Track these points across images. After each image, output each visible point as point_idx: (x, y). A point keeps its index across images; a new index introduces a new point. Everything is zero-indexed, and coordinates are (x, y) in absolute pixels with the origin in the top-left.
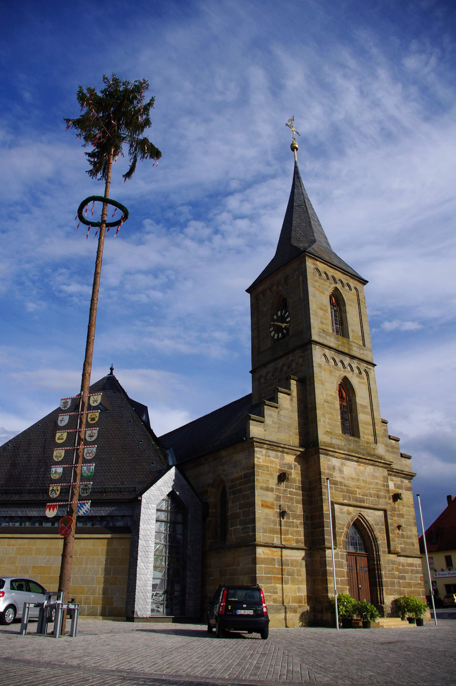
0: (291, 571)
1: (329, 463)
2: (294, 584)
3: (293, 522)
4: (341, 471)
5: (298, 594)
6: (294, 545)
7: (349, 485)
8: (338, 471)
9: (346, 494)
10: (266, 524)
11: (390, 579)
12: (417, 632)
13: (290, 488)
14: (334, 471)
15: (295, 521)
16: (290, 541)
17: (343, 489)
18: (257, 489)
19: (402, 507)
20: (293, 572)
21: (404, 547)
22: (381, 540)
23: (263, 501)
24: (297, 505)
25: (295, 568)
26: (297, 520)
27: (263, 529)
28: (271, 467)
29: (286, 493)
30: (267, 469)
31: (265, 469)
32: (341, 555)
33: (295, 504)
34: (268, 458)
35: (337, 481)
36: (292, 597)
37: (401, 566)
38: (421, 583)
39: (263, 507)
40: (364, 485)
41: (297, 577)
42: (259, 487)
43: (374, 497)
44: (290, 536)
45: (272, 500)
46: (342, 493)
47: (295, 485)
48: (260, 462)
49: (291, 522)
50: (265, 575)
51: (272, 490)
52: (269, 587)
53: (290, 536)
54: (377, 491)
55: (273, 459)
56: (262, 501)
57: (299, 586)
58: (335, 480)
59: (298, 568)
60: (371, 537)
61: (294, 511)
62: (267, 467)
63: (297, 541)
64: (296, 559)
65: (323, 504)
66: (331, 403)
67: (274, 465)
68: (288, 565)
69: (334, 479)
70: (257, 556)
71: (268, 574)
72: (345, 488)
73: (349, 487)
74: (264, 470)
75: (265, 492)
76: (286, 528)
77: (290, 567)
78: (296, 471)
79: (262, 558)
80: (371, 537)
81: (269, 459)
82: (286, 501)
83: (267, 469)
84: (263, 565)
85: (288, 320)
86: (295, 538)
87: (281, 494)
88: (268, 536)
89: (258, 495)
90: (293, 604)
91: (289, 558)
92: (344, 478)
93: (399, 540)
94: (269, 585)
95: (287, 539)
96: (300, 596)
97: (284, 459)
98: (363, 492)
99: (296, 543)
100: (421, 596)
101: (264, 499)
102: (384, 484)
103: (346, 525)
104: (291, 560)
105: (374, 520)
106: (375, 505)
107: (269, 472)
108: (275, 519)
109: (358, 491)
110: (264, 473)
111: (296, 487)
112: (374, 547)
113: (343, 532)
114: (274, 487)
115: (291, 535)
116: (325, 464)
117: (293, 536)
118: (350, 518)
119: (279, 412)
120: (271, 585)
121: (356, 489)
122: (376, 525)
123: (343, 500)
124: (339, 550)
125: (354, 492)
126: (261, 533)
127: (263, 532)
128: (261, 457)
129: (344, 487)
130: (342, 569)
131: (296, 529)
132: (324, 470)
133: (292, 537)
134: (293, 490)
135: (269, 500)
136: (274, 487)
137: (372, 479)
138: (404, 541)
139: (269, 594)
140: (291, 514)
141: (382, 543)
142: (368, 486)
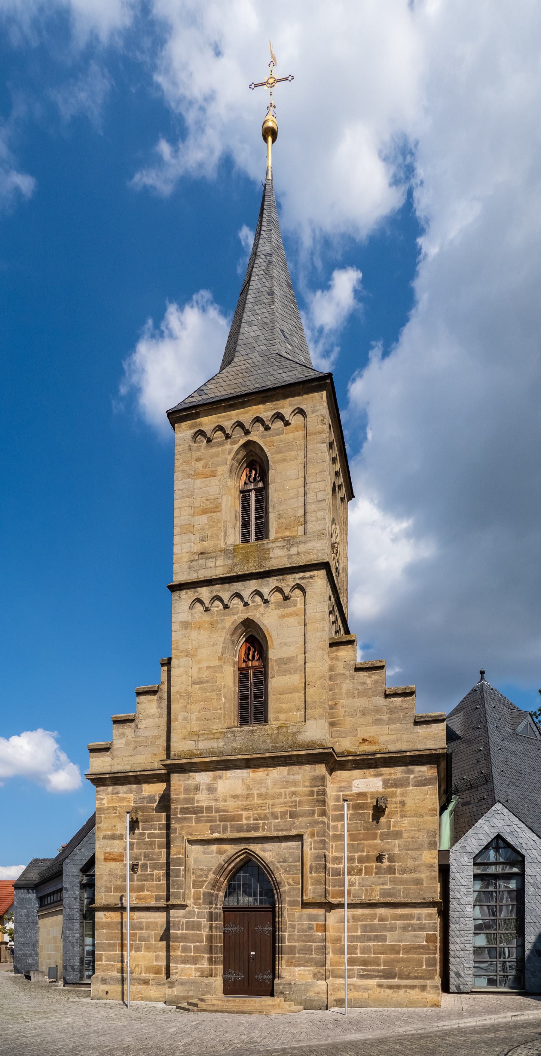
0: (146, 935)
1: (187, 782)
2: (149, 952)
3: (152, 874)
4: (211, 789)
5: (155, 963)
6: (153, 903)
7: (227, 808)
8: (206, 792)
9: (218, 823)
10: (111, 881)
11: (302, 944)
13: (150, 829)
14: (198, 792)
15: (156, 872)
16: (146, 899)
17: (211, 817)
18: (98, 840)
19: (399, 819)
20: (149, 937)
21: (390, 889)
22: (289, 884)
23: (107, 853)
24: (161, 850)
25: (153, 932)
26: (158, 870)
27: (106, 887)
28: (120, 807)
29: (143, 838)
30: (115, 811)
31: (111, 811)
32: (198, 912)
33: (157, 850)
34: (116, 795)
35: (202, 808)
36: (145, 966)
37: (377, 920)
38: (428, 946)
39: (106, 861)
40: (259, 802)
41: (155, 943)
42: (101, 837)
43: (281, 818)
44: (146, 893)
45: (120, 850)
46: (209, 824)
47: (159, 824)
48: (104, 804)
49: (148, 874)
50: (107, 942)
52: (112, 955)
53: (146, 893)
54: (290, 806)
55: (124, 796)
56: (105, 853)
57: (157, 953)
58: (197, 807)
59: (157, 932)
60: (272, 882)
61: (155, 860)
62: (115, 808)
63: (158, 898)
64: (155, 920)
65: (171, 846)
66: (208, 681)
67: (125, 803)
68: (142, 929)
69: (196, 805)
70: (96, 920)
71: (111, 941)
72: (217, 814)
73: (227, 811)
74: (109, 813)
75: (110, 842)
76: (140, 883)
77: (144, 931)
78: (161, 804)
79: (102, 922)
80: (272, 882)
81: (118, 796)
82: (143, 847)
83: (115, 811)
84: (104, 931)
86: (154, 894)
87: (135, 839)
88: (113, 895)
89: (100, 848)
90: (147, 975)
91: (143, 920)
92: (216, 800)
93: (379, 878)
94: (111, 953)
95: (141, 897)
96: (158, 965)
97: (142, 791)
98: (258, 814)
99: (155, 901)
100: (424, 967)
101: (108, 850)
102: (313, 792)
103: (213, 870)
104: (147, 922)
105: (278, 854)
106: (282, 830)
107: (117, 814)
108: (123, 873)
109: (245, 814)
110: (109, 817)
111: (161, 826)
112: (276, 897)
113: (205, 881)
115: (148, 890)
116: (180, 785)
117: (152, 892)
118: (222, 858)
119: (137, 726)
120: (115, 953)
121: (240, 812)
122: (279, 862)
123: (211, 834)
124: (195, 907)
125: (240, 817)
126: (102, 893)
127: (105, 892)
128: (106, 797)
129: (216, 812)
130: (198, 932)
131: (157, 882)
132: (177, 795)
133: (150, 893)
134: (156, 832)
135: (116, 850)
137: (281, 788)
138: (395, 878)
139: (112, 963)
140: (150, 863)
141: (290, 889)
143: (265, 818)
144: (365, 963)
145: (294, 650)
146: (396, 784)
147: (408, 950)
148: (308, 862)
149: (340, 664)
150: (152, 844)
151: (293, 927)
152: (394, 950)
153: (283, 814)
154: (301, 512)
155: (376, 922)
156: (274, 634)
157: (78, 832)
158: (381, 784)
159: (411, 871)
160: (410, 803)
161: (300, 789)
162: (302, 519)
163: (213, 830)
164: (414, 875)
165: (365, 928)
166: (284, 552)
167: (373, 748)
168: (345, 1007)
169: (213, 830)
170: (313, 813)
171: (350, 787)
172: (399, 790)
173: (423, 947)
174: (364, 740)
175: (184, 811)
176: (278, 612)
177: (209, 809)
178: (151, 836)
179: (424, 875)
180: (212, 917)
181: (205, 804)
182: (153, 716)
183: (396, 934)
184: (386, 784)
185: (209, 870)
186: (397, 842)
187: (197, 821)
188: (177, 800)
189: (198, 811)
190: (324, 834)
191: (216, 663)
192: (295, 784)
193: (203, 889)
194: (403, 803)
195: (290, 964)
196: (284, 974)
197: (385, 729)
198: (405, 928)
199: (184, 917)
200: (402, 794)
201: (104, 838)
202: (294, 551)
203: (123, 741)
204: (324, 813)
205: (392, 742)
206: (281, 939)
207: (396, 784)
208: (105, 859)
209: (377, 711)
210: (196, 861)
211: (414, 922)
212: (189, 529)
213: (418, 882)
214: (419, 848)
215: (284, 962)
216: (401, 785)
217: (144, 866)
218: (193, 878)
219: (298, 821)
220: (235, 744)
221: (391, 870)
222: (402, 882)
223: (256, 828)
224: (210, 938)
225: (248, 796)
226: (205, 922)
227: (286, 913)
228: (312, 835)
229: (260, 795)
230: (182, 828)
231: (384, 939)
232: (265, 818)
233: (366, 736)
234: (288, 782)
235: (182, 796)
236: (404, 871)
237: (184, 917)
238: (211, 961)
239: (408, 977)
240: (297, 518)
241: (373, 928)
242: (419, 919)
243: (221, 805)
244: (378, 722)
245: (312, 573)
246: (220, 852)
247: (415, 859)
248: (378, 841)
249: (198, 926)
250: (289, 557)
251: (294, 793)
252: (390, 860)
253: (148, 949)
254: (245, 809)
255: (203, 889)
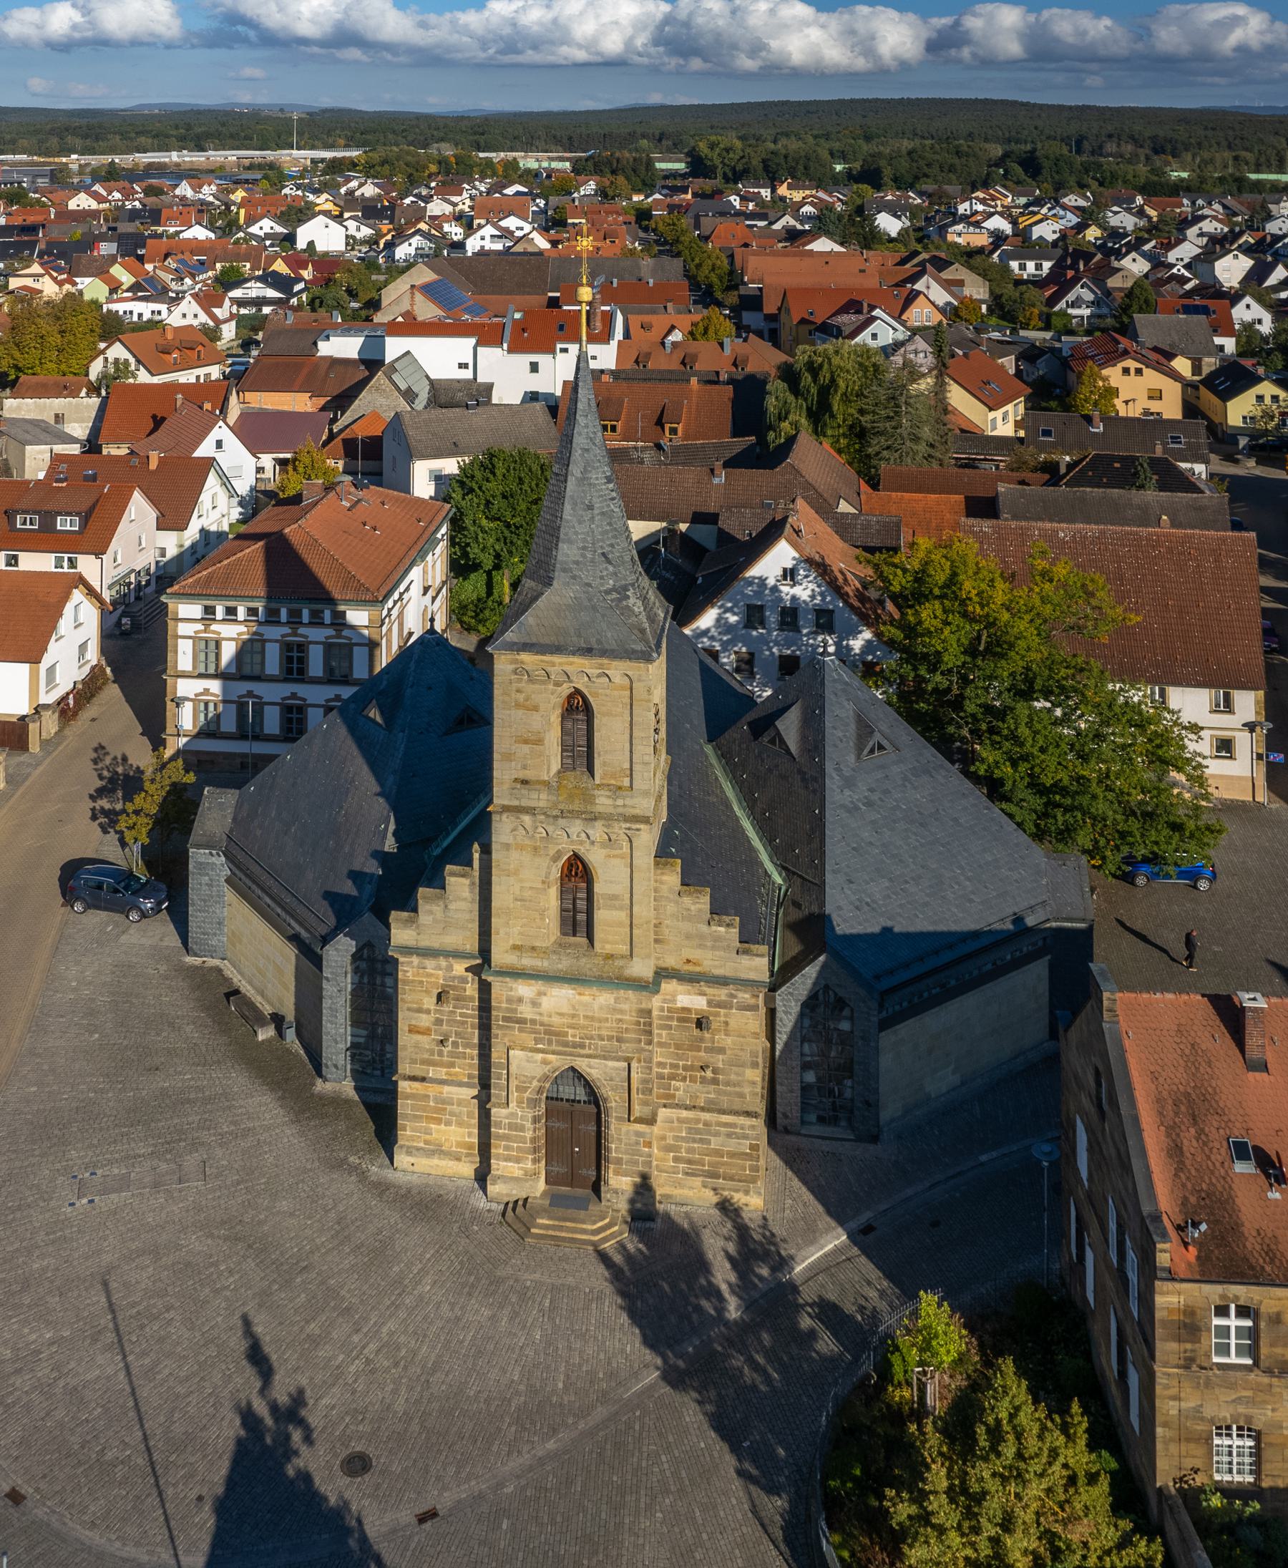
4: (535, 1004)
12: (954, 1089)
51: (428, 1012)
63: (470, 1076)
85: (301, 286)
92: (541, 1014)
109: (571, 1031)
114: (432, 1007)
136: (432, 1007)
142: (597, 1025)
143: (591, 1038)
144: (689, 1162)
145: (621, 888)
146: (720, 1005)
147: (732, 1155)
148: (634, 1085)
149: (665, 887)
150: (464, 1023)
151: (620, 1140)
152: (718, 1153)
153: (610, 1038)
154: (627, 765)
155: (701, 1126)
156: (600, 871)
157: (83, 110)
158: (705, 1002)
159: (734, 1085)
160: (733, 1024)
161: (627, 1017)
162: (628, 772)
163: (537, 1041)
164: (737, 1089)
165: (690, 1130)
166: (610, 802)
167: (698, 969)
168: (577, 339)
169: (537, 1041)
170: (640, 1041)
171: (674, 1001)
172: (722, 1011)
173: (747, 1154)
174: (688, 961)
175: (505, 1019)
176: (604, 852)
177: (533, 1022)
178: (462, 1015)
179: (747, 1090)
180: (536, 1120)
181: (529, 1017)
182: (465, 899)
183: (720, 1139)
184: (710, 1003)
185: (534, 1078)
186: (721, 1057)
187: (521, 1030)
188: (499, 1009)
189: (522, 1021)
190: (650, 1061)
191: (540, 886)
192: (622, 1012)
193: (527, 1095)
194: (726, 1023)
195: (617, 1173)
196: (611, 1182)
197: (709, 954)
198: (729, 1135)
199: (507, 1117)
200: (726, 1016)
201: (409, 1009)
202: (620, 802)
203: (431, 918)
204: (650, 1043)
205: (716, 967)
206: (608, 1149)
207: (720, 1005)
208: (410, 1031)
209: (701, 937)
210: (518, 1067)
211: (738, 1130)
212: (508, 757)
213: (742, 1095)
214: (743, 1065)
215: (611, 1171)
216: (725, 1007)
217: (455, 1044)
218: (516, 1083)
219: (624, 1046)
220: (560, 966)
221: (715, 1081)
222: (725, 1093)
223: (582, 1046)
224: (533, 1140)
225: (573, 1016)
226: (529, 1125)
227: (612, 1127)
228: (639, 1061)
229: (586, 1017)
230: (505, 1035)
231: (709, 1142)
232: (591, 1038)
233: (690, 957)
234: (614, 1010)
235: (504, 1005)
236: (728, 1084)
237: (507, 1117)
238: (535, 1161)
239: (732, 1179)
240: (623, 770)
241: (698, 1131)
242: (742, 1128)
243: (546, 1019)
244: (700, 946)
245: (638, 826)
246: (545, 1062)
247: (737, 1074)
248: (702, 1054)
249: (522, 1129)
250: (616, 807)
251: (620, 1020)
252: (714, 1072)
253: (460, 1124)
254: (571, 1027)
255: (527, 1095)
